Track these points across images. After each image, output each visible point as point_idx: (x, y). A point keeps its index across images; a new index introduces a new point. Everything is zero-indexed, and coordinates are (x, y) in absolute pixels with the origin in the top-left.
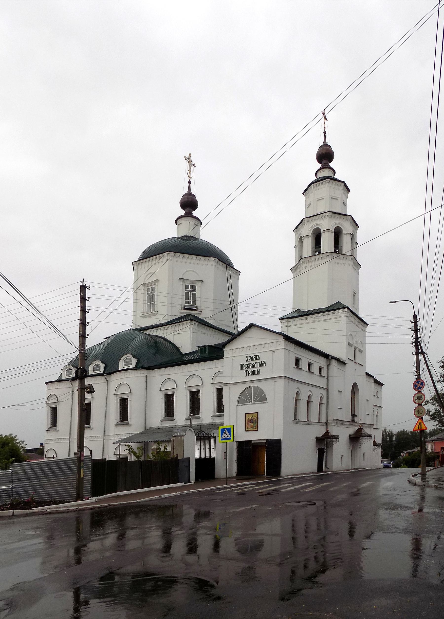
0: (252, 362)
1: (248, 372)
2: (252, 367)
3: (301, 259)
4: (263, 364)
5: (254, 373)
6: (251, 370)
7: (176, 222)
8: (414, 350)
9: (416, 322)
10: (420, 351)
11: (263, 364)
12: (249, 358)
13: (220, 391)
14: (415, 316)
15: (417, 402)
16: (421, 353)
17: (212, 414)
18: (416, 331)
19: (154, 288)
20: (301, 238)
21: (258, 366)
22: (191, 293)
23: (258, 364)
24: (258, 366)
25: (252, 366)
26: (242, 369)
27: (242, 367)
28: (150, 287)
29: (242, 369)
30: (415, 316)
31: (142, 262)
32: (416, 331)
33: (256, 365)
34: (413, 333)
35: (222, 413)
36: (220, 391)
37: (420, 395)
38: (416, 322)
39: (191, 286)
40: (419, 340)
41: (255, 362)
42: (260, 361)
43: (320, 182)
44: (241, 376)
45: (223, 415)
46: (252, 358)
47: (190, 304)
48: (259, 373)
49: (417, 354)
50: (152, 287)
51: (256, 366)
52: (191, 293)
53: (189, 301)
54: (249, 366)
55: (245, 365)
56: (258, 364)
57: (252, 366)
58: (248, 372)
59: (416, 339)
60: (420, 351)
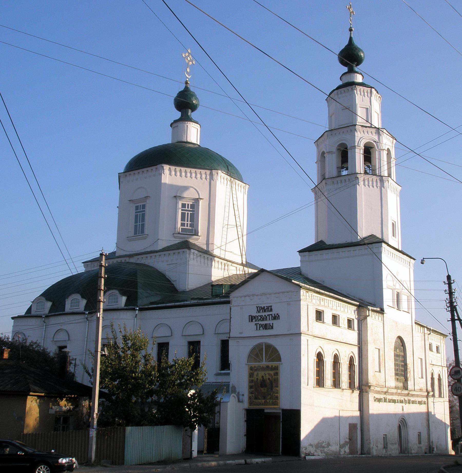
0: (263, 314)
1: (258, 325)
2: (263, 320)
3: (323, 178)
4: (276, 317)
5: (266, 327)
6: (260, 322)
7: (171, 125)
8: (449, 315)
9: (450, 284)
10: (456, 318)
11: (276, 317)
12: (260, 309)
13: (225, 345)
14: (449, 277)
15: (455, 377)
16: (457, 320)
17: (215, 372)
18: (451, 293)
19: (144, 206)
20: (323, 153)
21: (271, 319)
22: (188, 213)
23: (271, 316)
24: (271, 319)
25: (263, 319)
26: (252, 321)
27: (252, 318)
28: (139, 204)
29: (252, 321)
30: (449, 277)
31: (130, 174)
32: (451, 293)
33: (268, 317)
34: (447, 296)
35: (228, 371)
36: (225, 345)
37: (458, 369)
38: (450, 284)
39: (188, 205)
40: (455, 304)
41: (266, 314)
42: (272, 313)
43: (345, 89)
44: (250, 329)
45: (228, 374)
46: (264, 309)
47: (187, 226)
48: (272, 328)
49: (453, 320)
50: (142, 204)
51: (268, 319)
52: (188, 213)
53: (186, 222)
54: (259, 318)
55: (255, 317)
56: (271, 316)
57: (263, 319)
58: (258, 325)
59: (451, 303)
60: (456, 318)
